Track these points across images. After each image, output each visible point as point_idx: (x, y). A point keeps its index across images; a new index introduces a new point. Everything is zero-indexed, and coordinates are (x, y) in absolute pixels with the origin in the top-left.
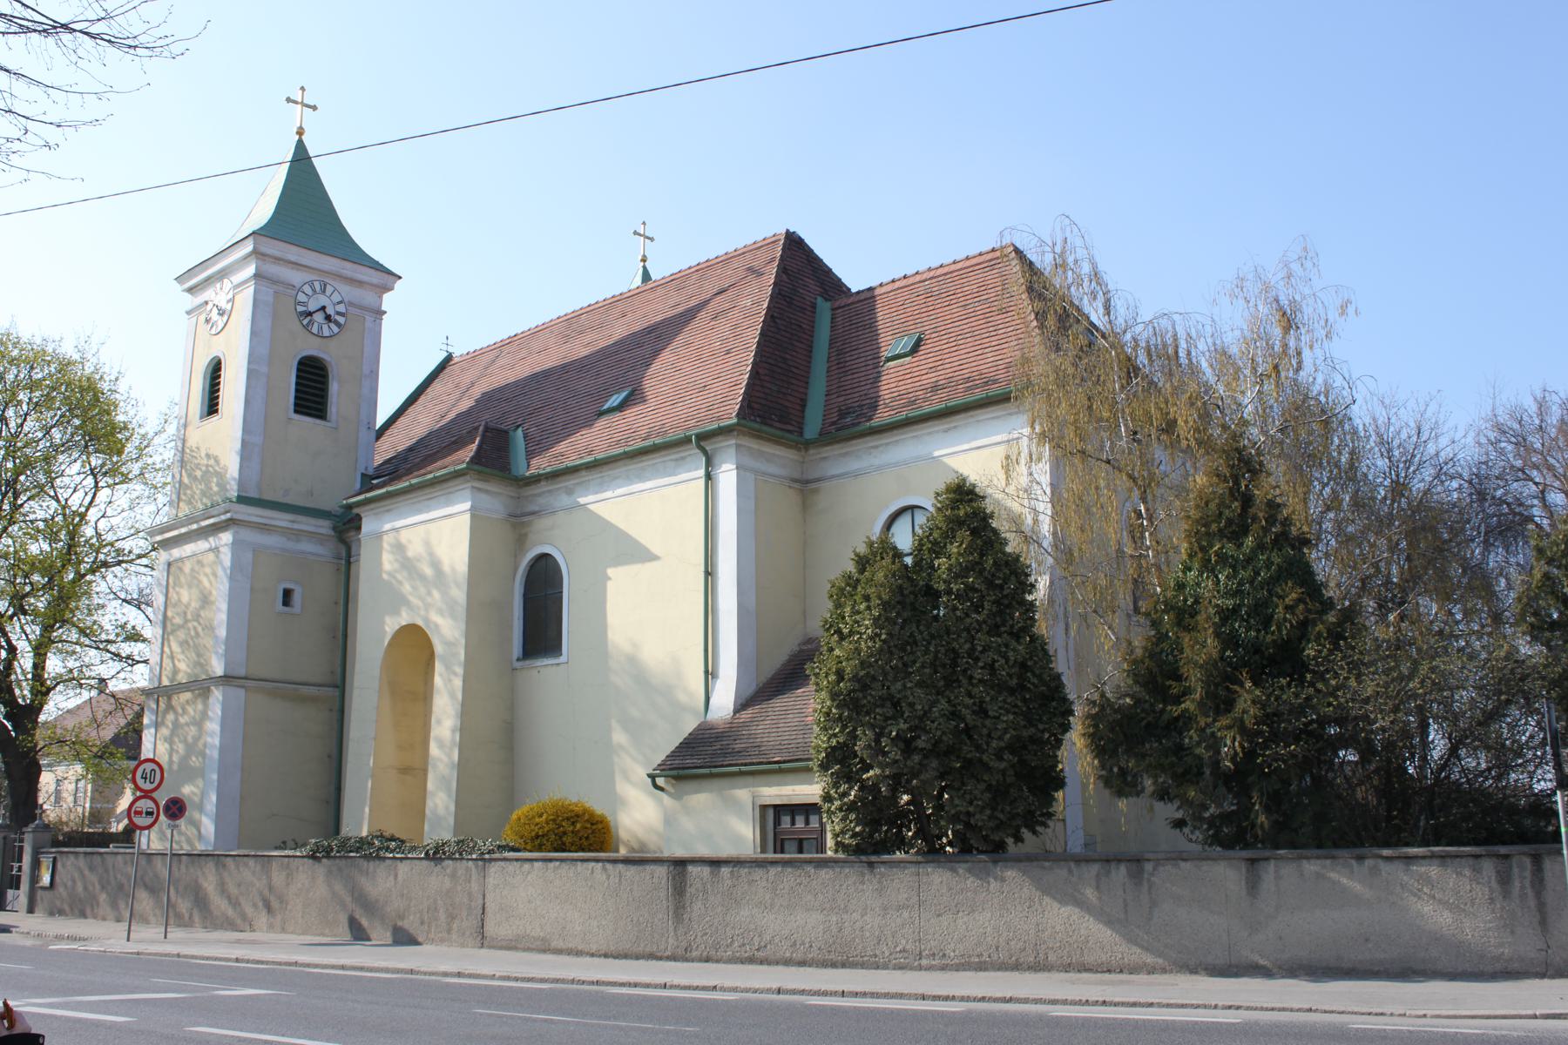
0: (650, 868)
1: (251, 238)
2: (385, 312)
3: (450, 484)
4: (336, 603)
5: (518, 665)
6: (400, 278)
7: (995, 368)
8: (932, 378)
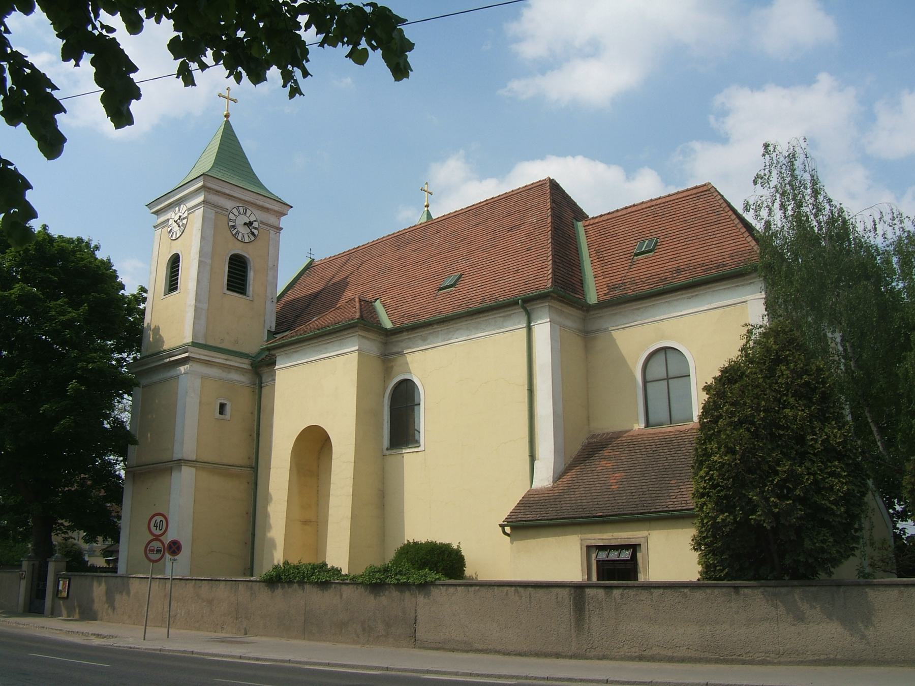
0: (555, 591)
1: (202, 177)
3: (344, 333)
4: (252, 413)
5: (387, 453)
6: (292, 207)
7: (722, 257)
8: (672, 265)
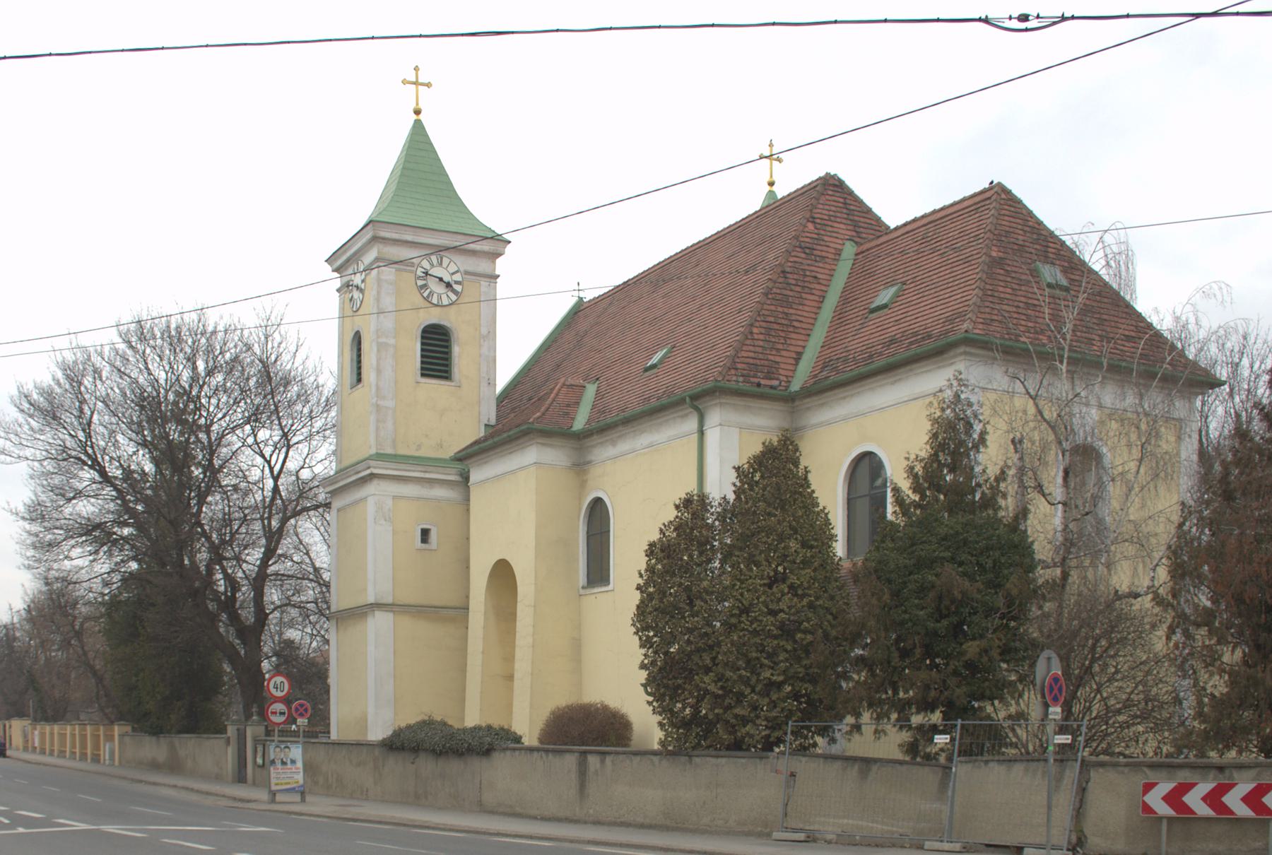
2: (499, 276)
5: (582, 592)
6: (510, 242)
